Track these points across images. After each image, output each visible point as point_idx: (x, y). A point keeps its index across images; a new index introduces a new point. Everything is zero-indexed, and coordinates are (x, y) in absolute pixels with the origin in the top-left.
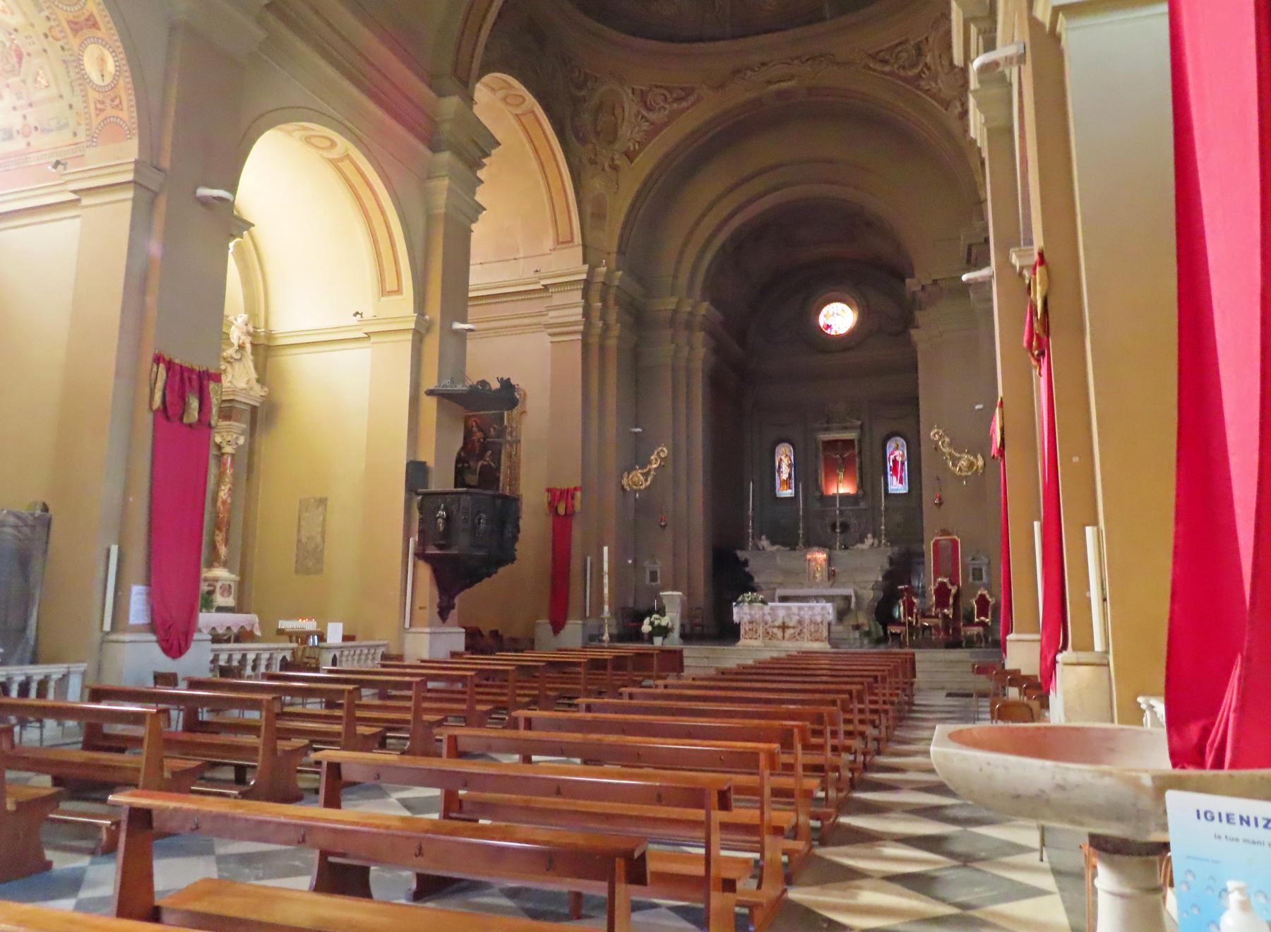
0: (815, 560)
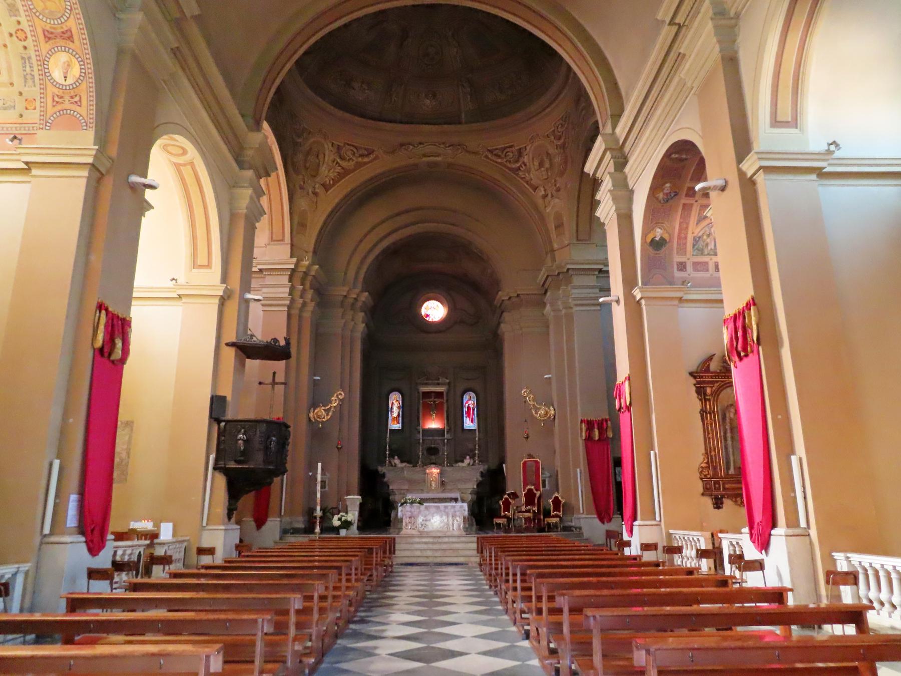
0: (432, 473)
